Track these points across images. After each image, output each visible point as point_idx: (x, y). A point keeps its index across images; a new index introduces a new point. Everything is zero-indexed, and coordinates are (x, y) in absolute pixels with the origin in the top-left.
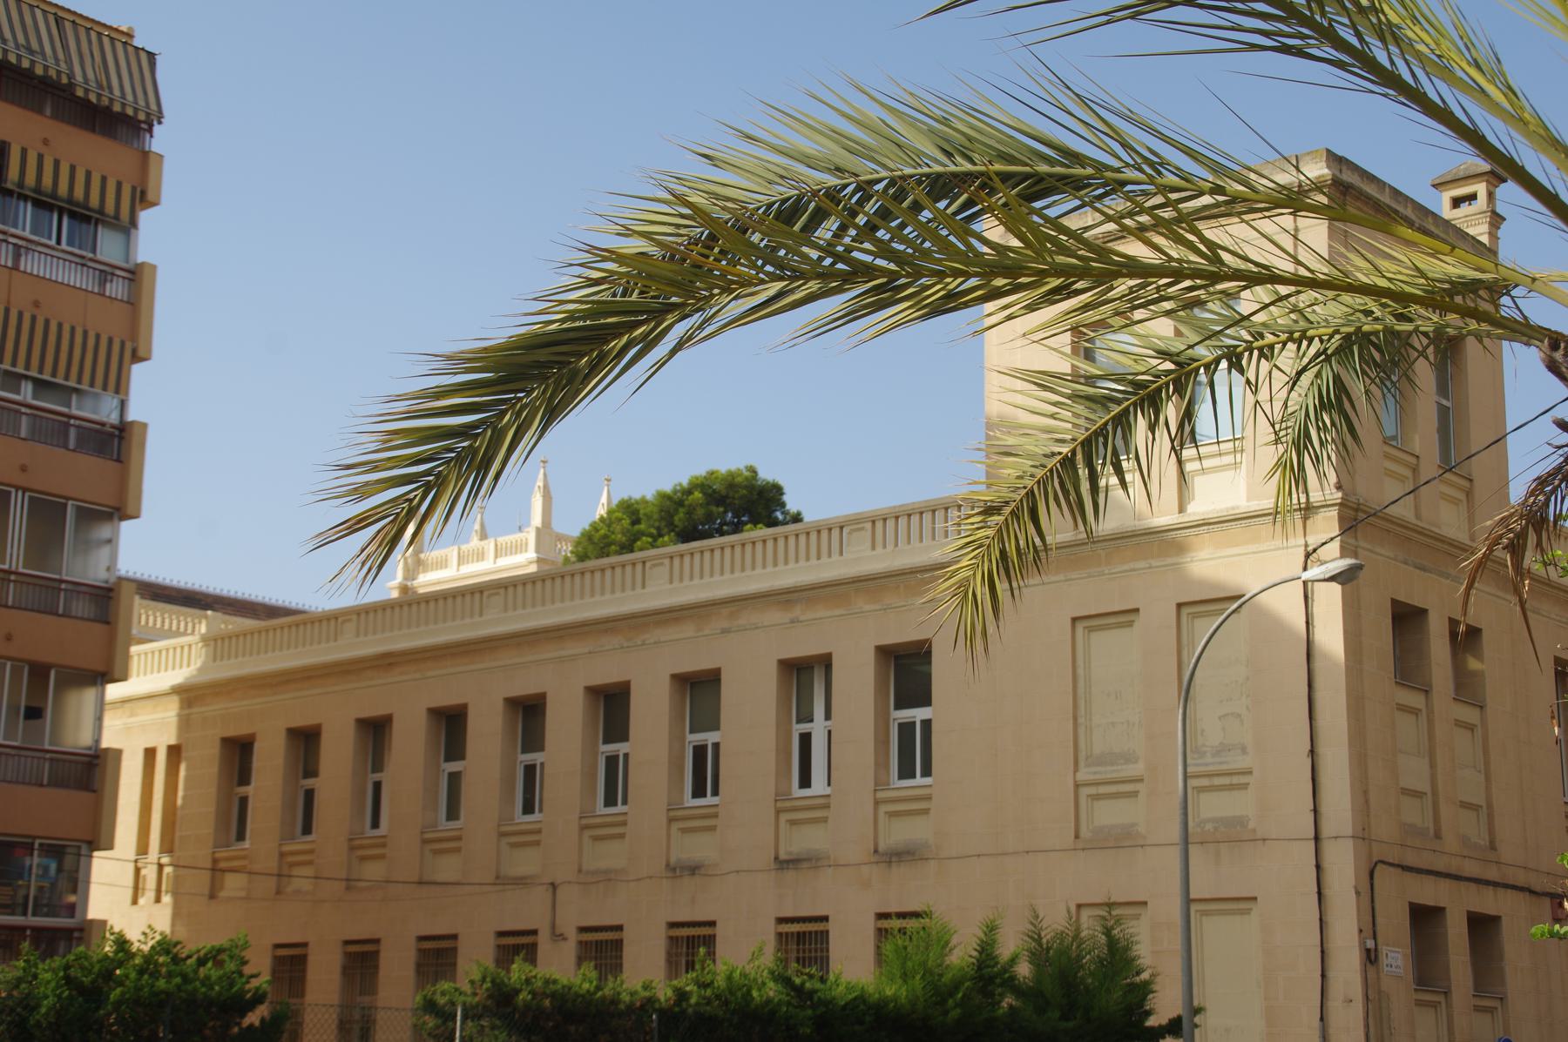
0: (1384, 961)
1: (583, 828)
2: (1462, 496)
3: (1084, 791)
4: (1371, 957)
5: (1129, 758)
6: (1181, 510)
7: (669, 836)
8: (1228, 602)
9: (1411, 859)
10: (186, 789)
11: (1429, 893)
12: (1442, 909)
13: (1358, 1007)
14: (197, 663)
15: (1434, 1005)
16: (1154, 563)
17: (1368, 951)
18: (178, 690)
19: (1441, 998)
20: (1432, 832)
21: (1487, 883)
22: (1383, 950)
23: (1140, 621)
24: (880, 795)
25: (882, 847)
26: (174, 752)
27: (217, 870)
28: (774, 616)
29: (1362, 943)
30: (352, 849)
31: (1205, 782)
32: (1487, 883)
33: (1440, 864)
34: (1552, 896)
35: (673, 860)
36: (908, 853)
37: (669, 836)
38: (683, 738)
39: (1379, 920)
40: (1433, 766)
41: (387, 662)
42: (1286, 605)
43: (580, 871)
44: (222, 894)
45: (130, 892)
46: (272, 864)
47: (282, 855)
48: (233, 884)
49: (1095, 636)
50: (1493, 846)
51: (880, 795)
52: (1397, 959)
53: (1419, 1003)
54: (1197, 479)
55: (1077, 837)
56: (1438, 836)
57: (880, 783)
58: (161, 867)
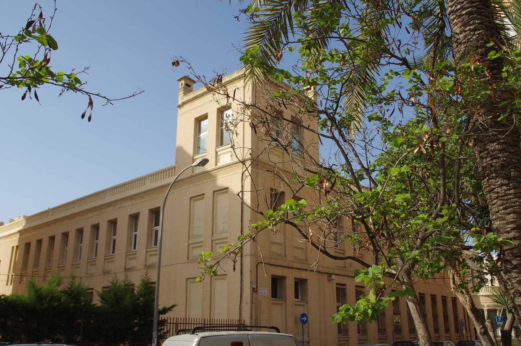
0: (260, 291)
1: (88, 262)
2: (281, 155)
3: (191, 246)
4: (254, 290)
5: (201, 236)
6: (216, 165)
7: (104, 263)
8: (226, 189)
9: (273, 262)
10: (19, 256)
11: (279, 272)
12: (285, 277)
13: (249, 305)
14: (23, 225)
15: (282, 304)
16: (209, 180)
17: (254, 289)
18: (19, 231)
19: (284, 302)
20: (284, 255)
21: (303, 269)
22: (260, 288)
23: (205, 196)
24: (148, 250)
25: (147, 265)
26: (17, 246)
27: (22, 276)
28: (129, 203)
29: (251, 286)
30: (46, 270)
31: (217, 242)
32: (303, 269)
33: (285, 264)
34: (327, 273)
35: (105, 270)
36: (152, 266)
37: (104, 263)
38: (111, 237)
39: (258, 279)
40: (285, 236)
41: (55, 221)
42: (236, 188)
43: (87, 274)
44: (22, 282)
45: (6, 282)
46: (31, 275)
47: (33, 272)
48: (25, 279)
49: (196, 202)
50: (306, 260)
51: (148, 250)
52: (265, 291)
53: (273, 304)
54: (221, 157)
55: (188, 259)
56: (285, 256)
57: (147, 247)
58: (12, 276)
